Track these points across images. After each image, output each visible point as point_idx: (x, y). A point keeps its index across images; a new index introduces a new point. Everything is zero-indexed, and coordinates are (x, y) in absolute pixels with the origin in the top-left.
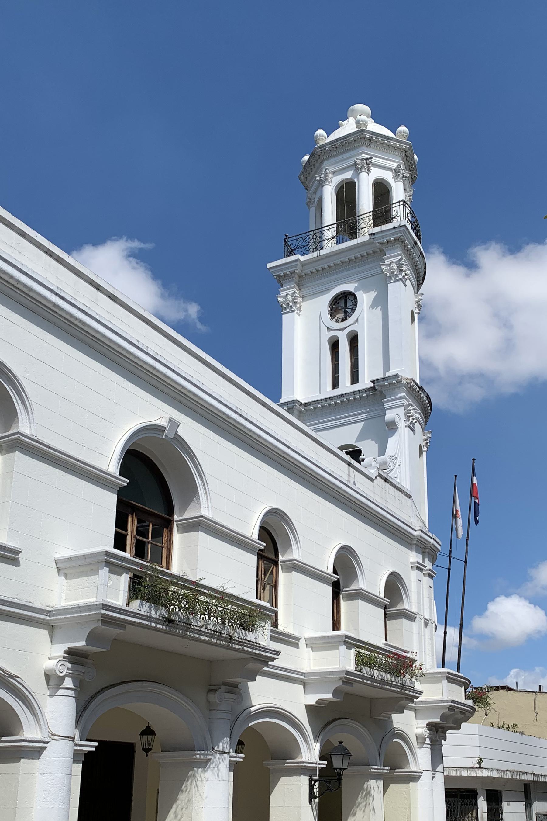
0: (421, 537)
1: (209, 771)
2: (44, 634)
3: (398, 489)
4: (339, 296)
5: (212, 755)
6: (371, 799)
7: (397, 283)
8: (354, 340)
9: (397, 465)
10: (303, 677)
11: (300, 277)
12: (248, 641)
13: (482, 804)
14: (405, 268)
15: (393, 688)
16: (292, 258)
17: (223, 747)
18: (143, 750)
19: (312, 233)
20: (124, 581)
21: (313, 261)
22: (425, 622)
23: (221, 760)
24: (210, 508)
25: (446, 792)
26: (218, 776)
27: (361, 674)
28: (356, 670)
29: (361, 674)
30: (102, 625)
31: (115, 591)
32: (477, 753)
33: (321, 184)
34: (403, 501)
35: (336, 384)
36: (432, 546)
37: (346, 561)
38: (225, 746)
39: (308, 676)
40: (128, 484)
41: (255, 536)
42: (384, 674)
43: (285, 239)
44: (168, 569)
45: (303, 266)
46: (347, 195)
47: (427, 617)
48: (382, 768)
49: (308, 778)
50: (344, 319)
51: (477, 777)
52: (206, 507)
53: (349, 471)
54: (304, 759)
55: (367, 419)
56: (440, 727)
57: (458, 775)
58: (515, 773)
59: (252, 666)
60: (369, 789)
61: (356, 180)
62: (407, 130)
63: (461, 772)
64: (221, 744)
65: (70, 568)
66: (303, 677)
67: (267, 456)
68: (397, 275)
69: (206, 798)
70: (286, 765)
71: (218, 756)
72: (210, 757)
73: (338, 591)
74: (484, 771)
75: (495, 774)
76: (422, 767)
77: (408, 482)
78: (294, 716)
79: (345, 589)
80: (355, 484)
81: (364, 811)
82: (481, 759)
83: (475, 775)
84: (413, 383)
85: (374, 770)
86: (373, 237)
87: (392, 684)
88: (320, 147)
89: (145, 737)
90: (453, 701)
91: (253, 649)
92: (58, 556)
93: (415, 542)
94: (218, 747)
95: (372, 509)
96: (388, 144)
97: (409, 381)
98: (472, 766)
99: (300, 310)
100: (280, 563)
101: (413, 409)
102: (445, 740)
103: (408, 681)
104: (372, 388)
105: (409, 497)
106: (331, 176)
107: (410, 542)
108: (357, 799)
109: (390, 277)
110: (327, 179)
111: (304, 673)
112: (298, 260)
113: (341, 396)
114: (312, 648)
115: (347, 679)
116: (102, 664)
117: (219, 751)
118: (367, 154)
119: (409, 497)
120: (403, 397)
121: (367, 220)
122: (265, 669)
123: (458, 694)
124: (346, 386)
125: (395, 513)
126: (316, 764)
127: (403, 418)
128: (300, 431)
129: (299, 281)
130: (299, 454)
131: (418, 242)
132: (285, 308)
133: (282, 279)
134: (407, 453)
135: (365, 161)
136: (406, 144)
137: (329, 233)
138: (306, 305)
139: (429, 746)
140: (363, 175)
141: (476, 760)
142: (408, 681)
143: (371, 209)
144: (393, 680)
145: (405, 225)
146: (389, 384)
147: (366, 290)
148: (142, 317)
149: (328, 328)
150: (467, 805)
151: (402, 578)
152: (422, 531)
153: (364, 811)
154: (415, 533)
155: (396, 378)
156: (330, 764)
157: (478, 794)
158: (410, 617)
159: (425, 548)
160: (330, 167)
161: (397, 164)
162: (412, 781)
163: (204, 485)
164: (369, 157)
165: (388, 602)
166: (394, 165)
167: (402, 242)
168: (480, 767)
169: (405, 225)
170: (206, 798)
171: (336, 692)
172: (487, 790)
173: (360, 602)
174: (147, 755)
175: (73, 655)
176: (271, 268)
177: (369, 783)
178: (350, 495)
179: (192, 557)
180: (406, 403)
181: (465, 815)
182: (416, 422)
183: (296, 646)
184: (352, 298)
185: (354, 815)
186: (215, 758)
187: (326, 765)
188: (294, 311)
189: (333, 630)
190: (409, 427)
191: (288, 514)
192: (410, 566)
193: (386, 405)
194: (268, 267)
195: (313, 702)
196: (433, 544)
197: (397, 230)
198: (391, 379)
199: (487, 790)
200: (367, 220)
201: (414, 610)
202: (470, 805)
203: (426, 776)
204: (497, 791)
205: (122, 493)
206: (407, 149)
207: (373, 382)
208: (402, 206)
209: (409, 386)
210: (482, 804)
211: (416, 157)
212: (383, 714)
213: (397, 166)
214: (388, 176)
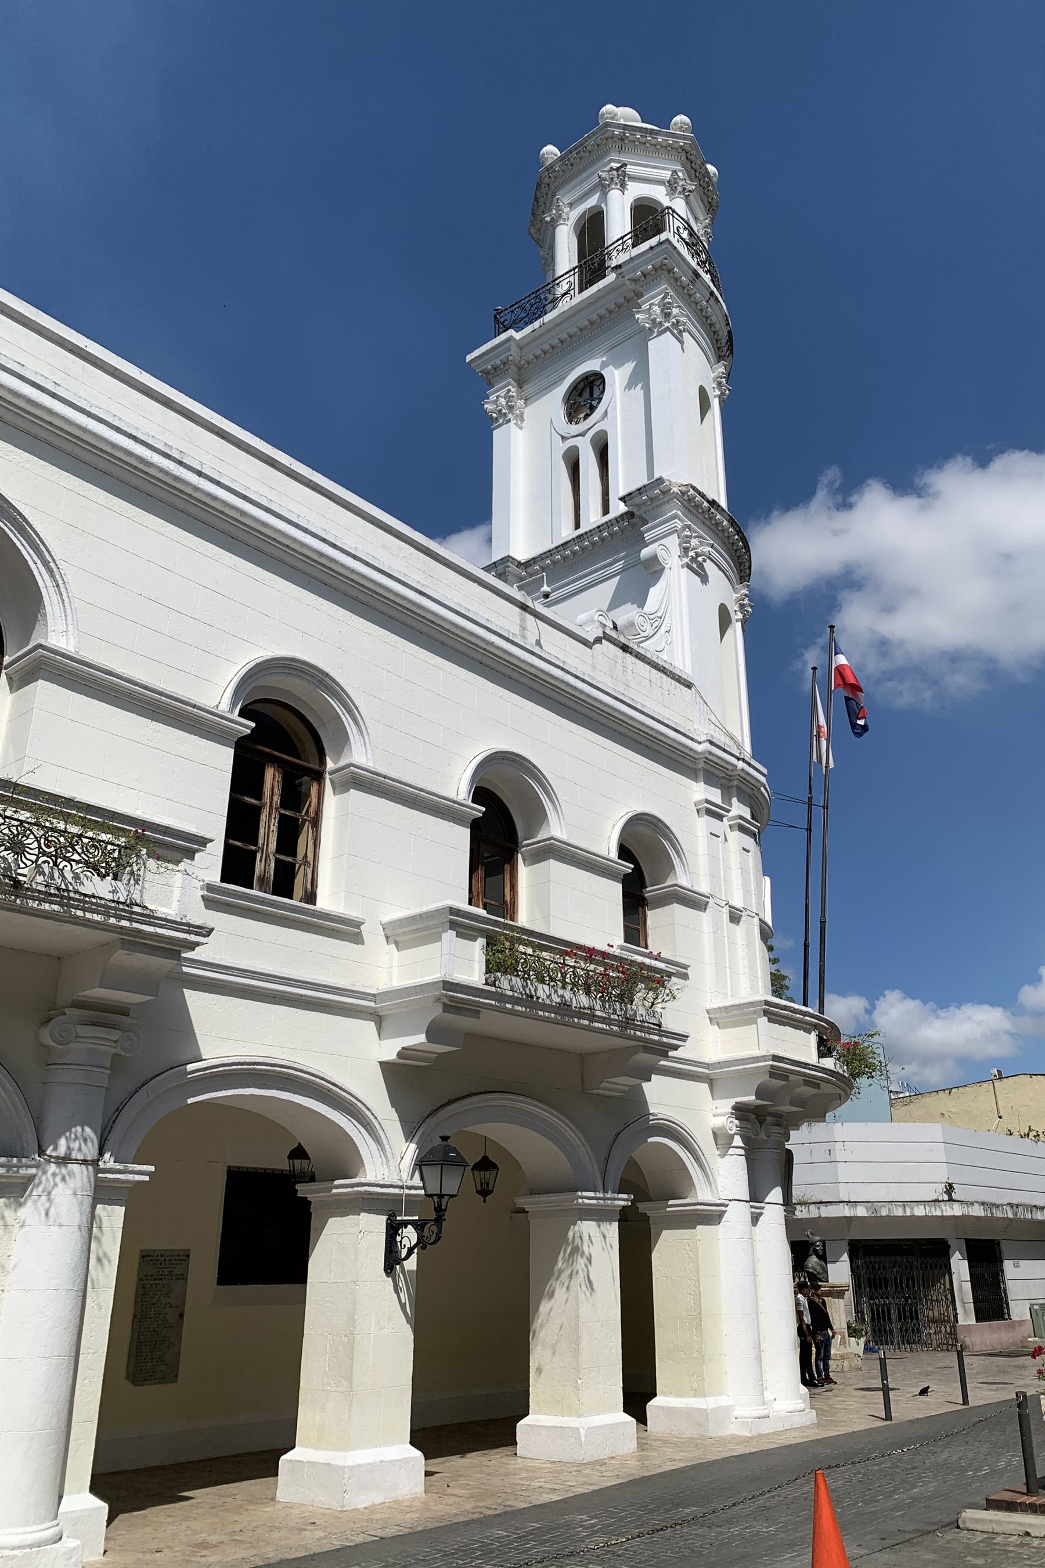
0: (710, 753)
1: (29, 1203)
2: (369, 1027)
3: (663, 670)
5: (37, 1166)
6: (581, 1262)
7: (661, 337)
9: (663, 630)
10: (372, 1004)
11: (520, 369)
12: (85, 895)
13: (960, 1267)
14: (675, 311)
15: (596, 1025)
16: (503, 337)
17: (69, 1148)
20: (813, 1038)
21: (535, 336)
22: (730, 912)
23: (58, 1179)
24: (71, 632)
26: (47, 1214)
27: (493, 989)
28: (487, 984)
29: (493, 989)
31: (467, 963)
32: (943, 1175)
33: (554, 224)
34: (673, 691)
36: (743, 774)
38: (75, 1145)
39: (382, 1001)
40: (484, 813)
41: (614, 854)
42: (568, 994)
43: (495, 317)
44: (512, 919)
45: (521, 348)
47: (738, 903)
48: (609, 1195)
49: (383, 1219)
51: (943, 1218)
52: (557, 828)
53: (523, 620)
54: (370, 1178)
55: (624, 570)
56: (771, 1114)
57: (908, 1214)
58: (1021, 1208)
59: (643, 1057)
60: (578, 1241)
61: (603, 205)
62: (687, 120)
63: (912, 1209)
64: (63, 1142)
65: (727, 1017)
66: (372, 1004)
67: (282, 561)
68: (660, 323)
69: (15, 1266)
70: (334, 1191)
71: (53, 1168)
72: (33, 1171)
73: (513, 846)
74: (956, 1206)
75: (977, 1211)
76: (723, 1195)
77: (688, 663)
78: (322, 1079)
79: (525, 842)
80: (538, 643)
81: (568, 1288)
82: (951, 1185)
83: (939, 1214)
84: (692, 492)
85: (586, 1201)
86: (619, 271)
87: (594, 1016)
88: (547, 169)
90: (775, 1058)
91: (84, 910)
92: (708, 1007)
93: (701, 765)
94: (55, 1149)
95: (582, 692)
96: (654, 142)
97: (684, 489)
98: (935, 1198)
99: (522, 420)
100: (327, 777)
101: (696, 537)
103: (642, 1011)
104: (626, 513)
105: (689, 685)
106: (567, 209)
108: (556, 1262)
109: (650, 329)
110: (560, 216)
111: (374, 995)
112: (510, 339)
114: (718, 1024)
117: (57, 1157)
118: (618, 161)
119: (689, 685)
120: (675, 517)
122: (663, 1063)
123: (802, 1048)
125: (592, 678)
126: (401, 1187)
127: (676, 551)
128: (372, 523)
129: (519, 376)
130: (367, 564)
132: (496, 419)
133: (490, 377)
134: (685, 610)
135: (614, 172)
136: (684, 138)
138: (529, 412)
139: (742, 1152)
140: (614, 194)
141: (941, 1188)
142: (642, 1011)
144: (597, 1007)
145: (667, 240)
146: (651, 499)
147: (618, 363)
148: (55, 338)
149: (563, 437)
150: (931, 1267)
151: (668, 828)
152: (711, 743)
153: (568, 1288)
154: (699, 748)
155: (659, 485)
157: (949, 1247)
158: (695, 902)
159: (729, 778)
160: (564, 198)
162: (702, 1224)
163: (58, 586)
165: (479, 811)
166: (667, 175)
167: (669, 272)
168: (951, 1200)
169: (667, 240)
170: (15, 1266)
171: (434, 1033)
172: (967, 1241)
173: (676, 907)
174: (485, 1201)
175: (741, 1111)
176: (472, 361)
177: (577, 1228)
178: (519, 659)
179: (568, 905)
180: (679, 525)
181: (934, 1285)
182: (704, 561)
183: (357, 938)
185: (551, 1295)
186: (45, 1173)
187: (632, 1201)
188: (509, 421)
190: (689, 567)
191: (332, 673)
192: (695, 809)
195: (391, 1056)
196: (743, 770)
197: (655, 251)
198: (651, 489)
199: (967, 1241)
201: (704, 889)
202: (936, 1267)
203: (737, 1214)
204: (993, 1241)
205: (476, 827)
206: (688, 148)
209: (686, 498)
210: (960, 1267)
211: (710, 168)
212: (603, 1085)
214: (659, 194)
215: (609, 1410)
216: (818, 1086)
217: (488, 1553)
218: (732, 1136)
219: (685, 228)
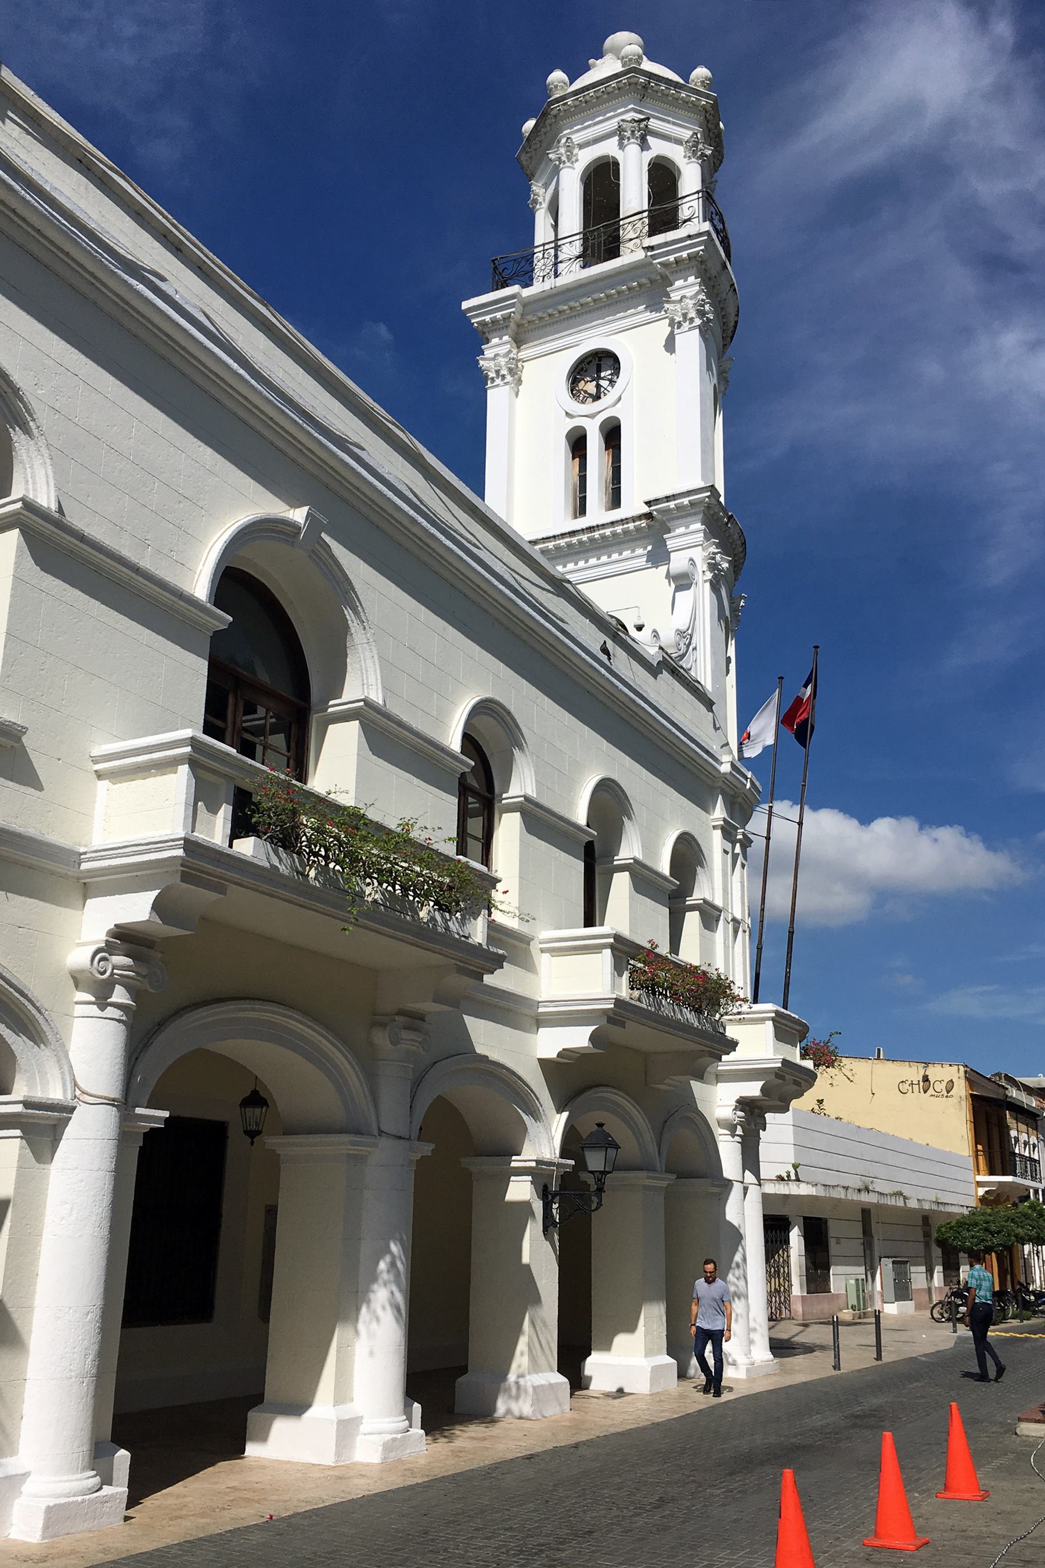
4: (586, 358)
8: (612, 435)
11: (518, 326)
18: (246, 1132)
19: (541, 248)
25: (764, 1220)
30: (182, 881)
35: (581, 509)
46: (602, 180)
47: (739, 916)
50: (597, 397)
58: (850, 1190)
89: (249, 1111)
102: (764, 1130)
107: (710, 783)
109: (679, 322)
113: (591, 529)
115: (619, 1013)
116: (169, 977)
118: (640, 112)
121: (639, 225)
124: (597, 513)
131: (728, 264)
136: (708, 96)
137: (572, 249)
143: (646, 207)
156: (581, 1164)
161: (691, 133)
164: (643, 117)
172: (805, 1218)
174: (252, 1143)
184: (610, 362)
193: (671, 544)
194: (463, 308)
199: (805, 1218)
200: (639, 225)
204: (820, 1219)
207: (648, 503)
213: (692, 137)
214: (676, 154)
215: (659, 1353)
216: (221, 890)
217: (126, 1565)
218: (736, 1126)
219: (717, 214)
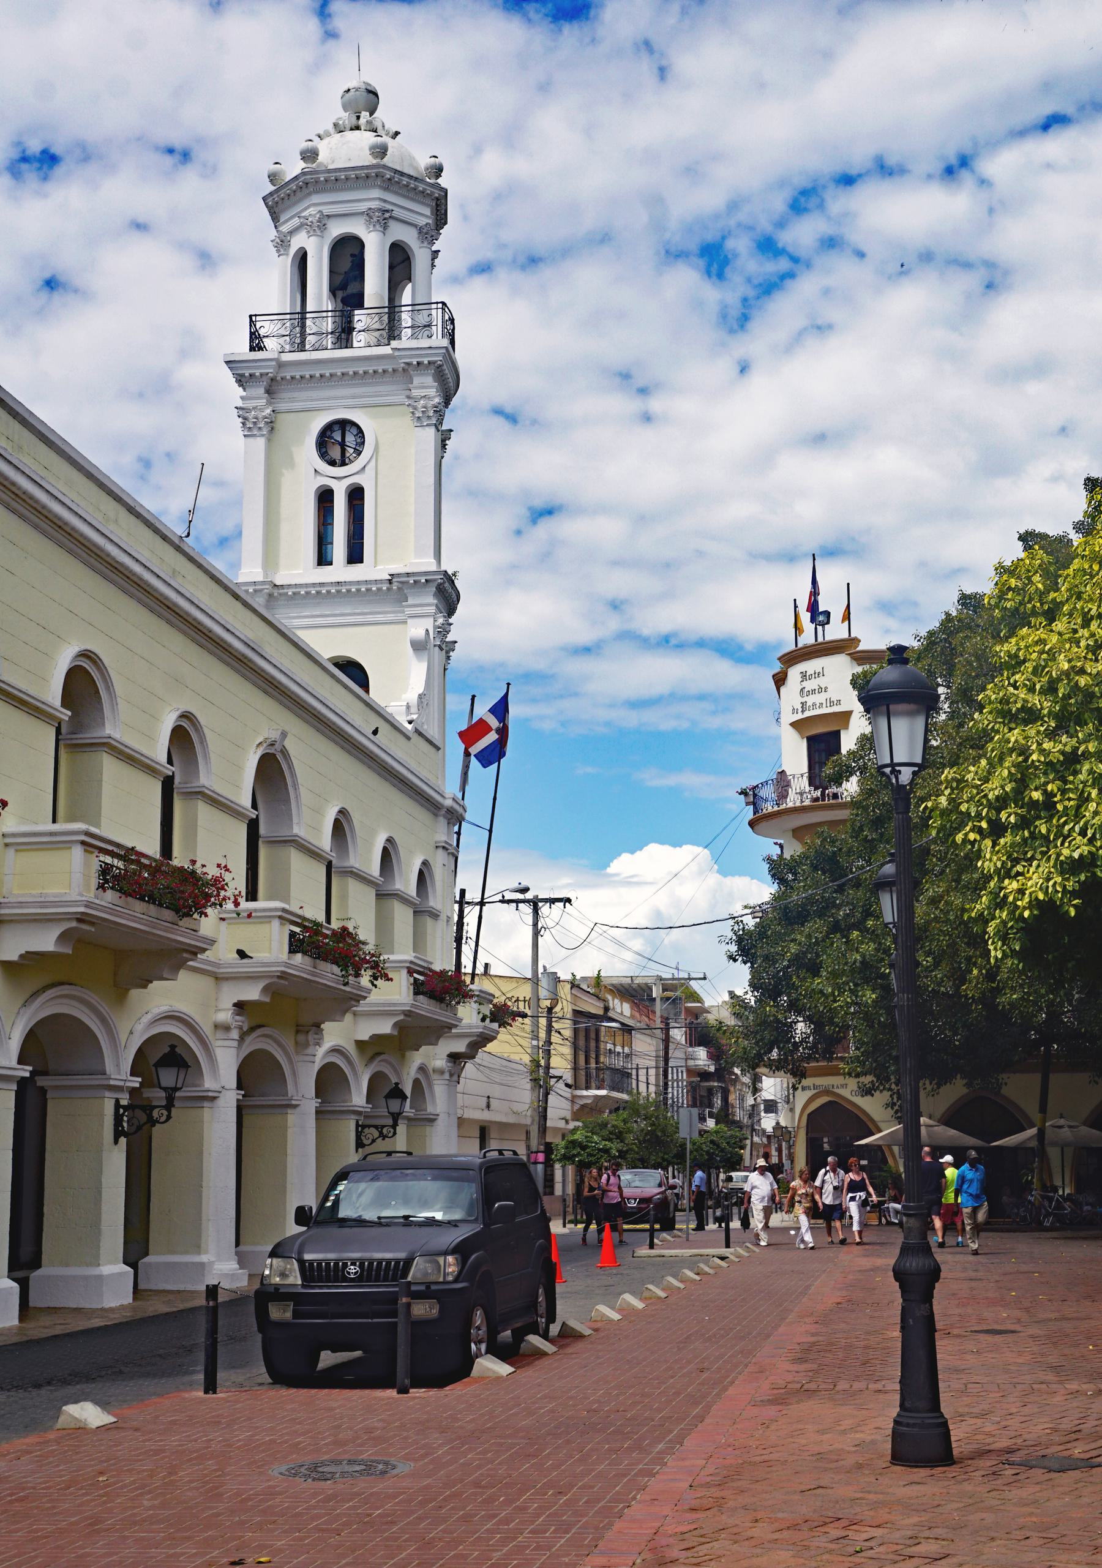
8: (356, 495)
37: (83, 685)
54: (354, 1103)
173: (293, 850)
189: (54, 821)
208: (440, 311)
